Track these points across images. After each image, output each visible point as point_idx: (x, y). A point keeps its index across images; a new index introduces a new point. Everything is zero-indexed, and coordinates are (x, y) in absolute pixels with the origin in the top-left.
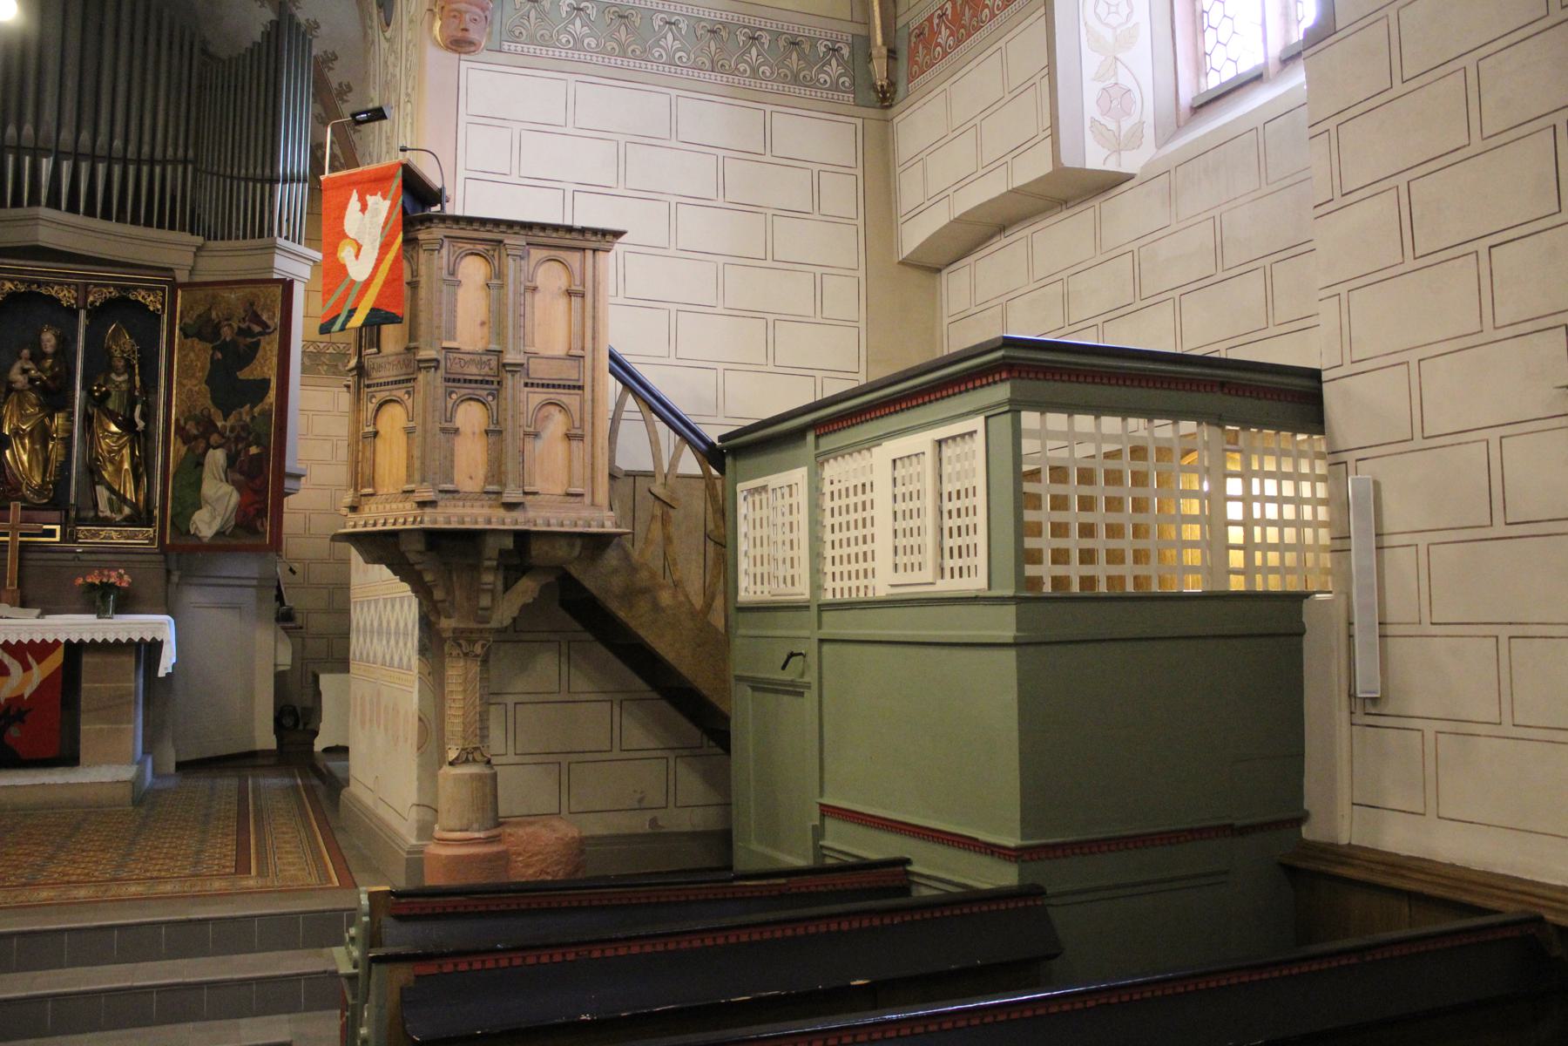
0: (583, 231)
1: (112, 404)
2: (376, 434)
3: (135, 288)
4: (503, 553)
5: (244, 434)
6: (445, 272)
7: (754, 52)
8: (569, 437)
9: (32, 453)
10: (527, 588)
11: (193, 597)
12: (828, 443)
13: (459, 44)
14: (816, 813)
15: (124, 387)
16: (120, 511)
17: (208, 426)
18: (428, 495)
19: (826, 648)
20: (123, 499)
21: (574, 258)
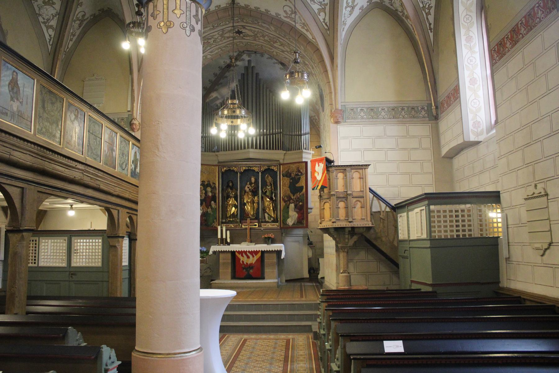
0: (362, 165)
1: (268, 194)
2: (324, 209)
3: (271, 166)
4: (349, 231)
5: (298, 200)
6: (335, 176)
7: (403, 112)
8: (361, 207)
9: (251, 206)
10: (355, 238)
11: (289, 239)
12: (410, 208)
13: (337, 122)
14: (410, 281)
15: (270, 189)
16: (271, 219)
17: (290, 198)
18: (334, 220)
19: (411, 249)
20: (271, 216)
21: (361, 171)
